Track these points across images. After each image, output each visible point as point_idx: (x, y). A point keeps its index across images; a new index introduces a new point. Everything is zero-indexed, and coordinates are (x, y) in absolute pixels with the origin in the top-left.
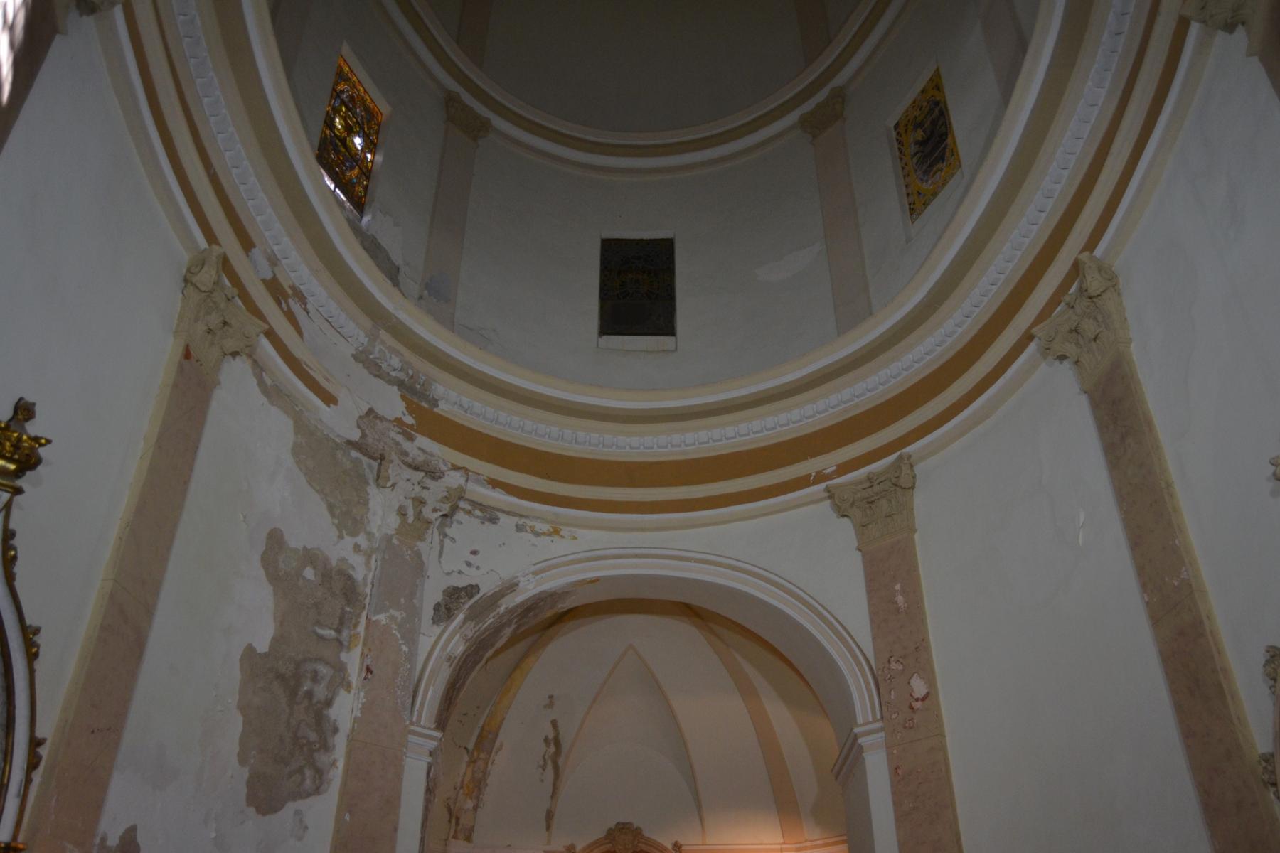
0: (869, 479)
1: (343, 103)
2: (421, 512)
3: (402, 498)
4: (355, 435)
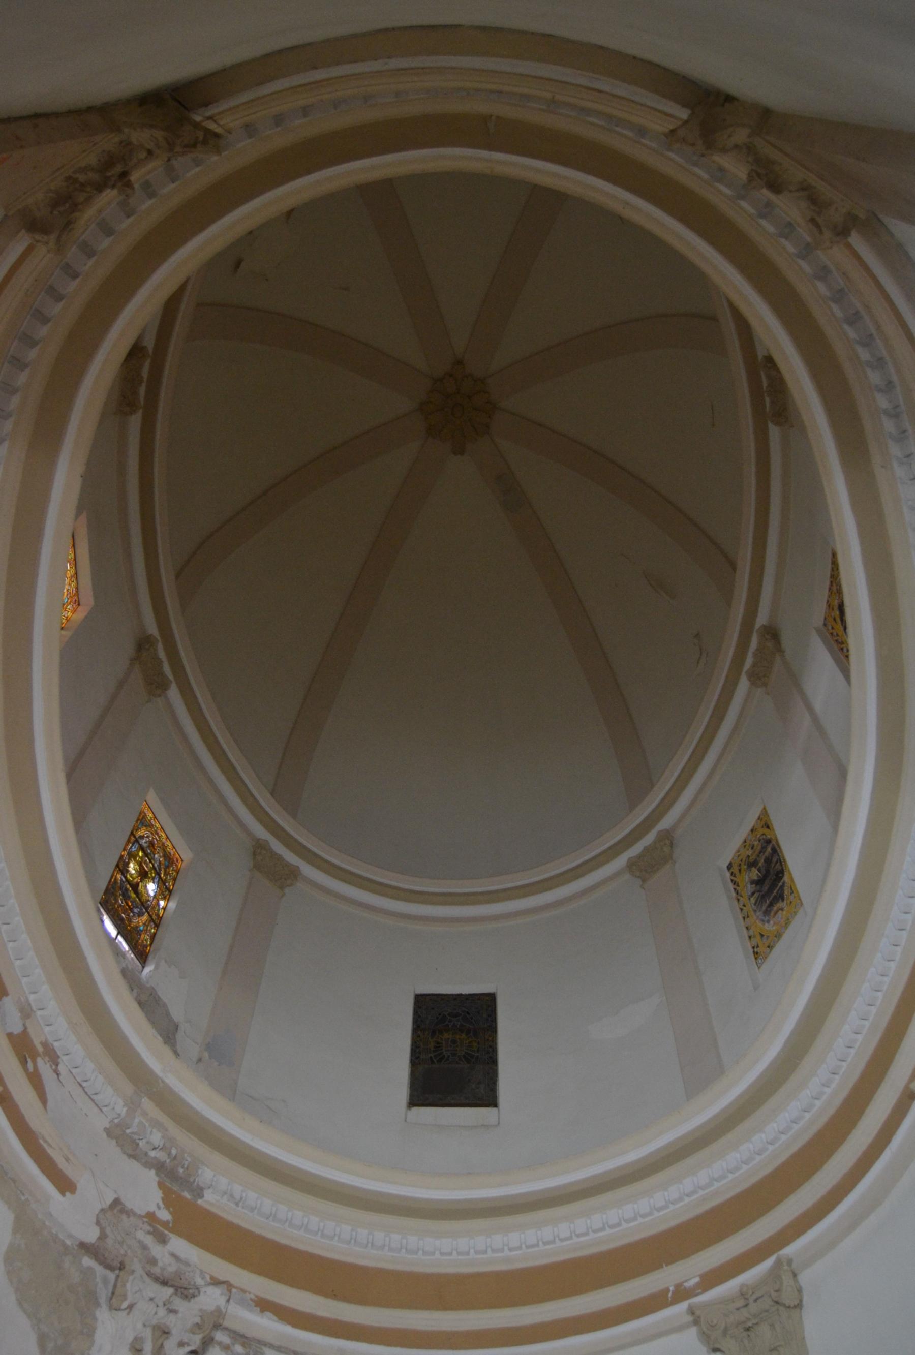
0: (743, 1293)
1: (142, 848)
2: (162, 1346)
3: (139, 1325)
4: (91, 1235)
